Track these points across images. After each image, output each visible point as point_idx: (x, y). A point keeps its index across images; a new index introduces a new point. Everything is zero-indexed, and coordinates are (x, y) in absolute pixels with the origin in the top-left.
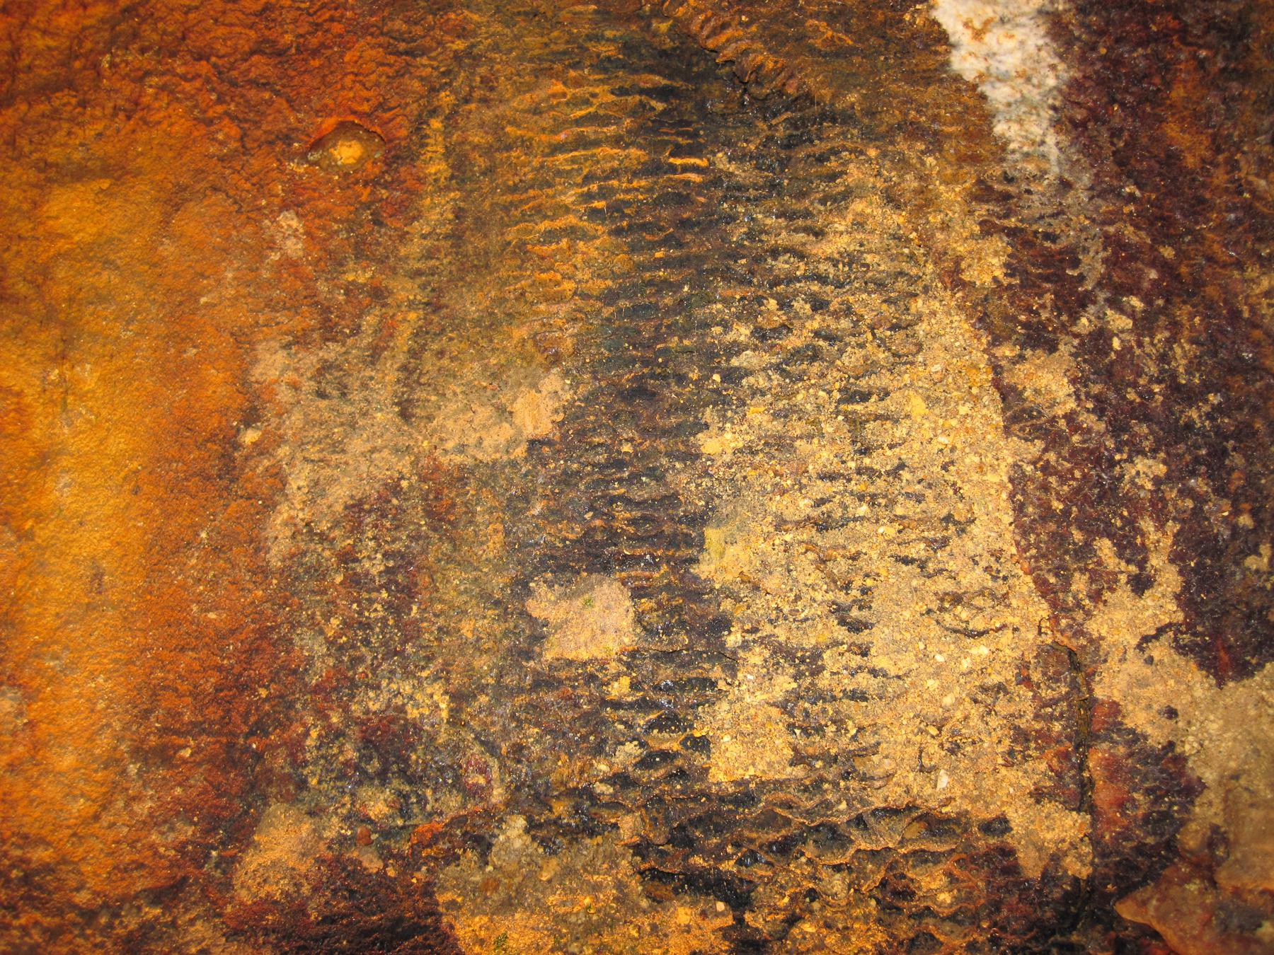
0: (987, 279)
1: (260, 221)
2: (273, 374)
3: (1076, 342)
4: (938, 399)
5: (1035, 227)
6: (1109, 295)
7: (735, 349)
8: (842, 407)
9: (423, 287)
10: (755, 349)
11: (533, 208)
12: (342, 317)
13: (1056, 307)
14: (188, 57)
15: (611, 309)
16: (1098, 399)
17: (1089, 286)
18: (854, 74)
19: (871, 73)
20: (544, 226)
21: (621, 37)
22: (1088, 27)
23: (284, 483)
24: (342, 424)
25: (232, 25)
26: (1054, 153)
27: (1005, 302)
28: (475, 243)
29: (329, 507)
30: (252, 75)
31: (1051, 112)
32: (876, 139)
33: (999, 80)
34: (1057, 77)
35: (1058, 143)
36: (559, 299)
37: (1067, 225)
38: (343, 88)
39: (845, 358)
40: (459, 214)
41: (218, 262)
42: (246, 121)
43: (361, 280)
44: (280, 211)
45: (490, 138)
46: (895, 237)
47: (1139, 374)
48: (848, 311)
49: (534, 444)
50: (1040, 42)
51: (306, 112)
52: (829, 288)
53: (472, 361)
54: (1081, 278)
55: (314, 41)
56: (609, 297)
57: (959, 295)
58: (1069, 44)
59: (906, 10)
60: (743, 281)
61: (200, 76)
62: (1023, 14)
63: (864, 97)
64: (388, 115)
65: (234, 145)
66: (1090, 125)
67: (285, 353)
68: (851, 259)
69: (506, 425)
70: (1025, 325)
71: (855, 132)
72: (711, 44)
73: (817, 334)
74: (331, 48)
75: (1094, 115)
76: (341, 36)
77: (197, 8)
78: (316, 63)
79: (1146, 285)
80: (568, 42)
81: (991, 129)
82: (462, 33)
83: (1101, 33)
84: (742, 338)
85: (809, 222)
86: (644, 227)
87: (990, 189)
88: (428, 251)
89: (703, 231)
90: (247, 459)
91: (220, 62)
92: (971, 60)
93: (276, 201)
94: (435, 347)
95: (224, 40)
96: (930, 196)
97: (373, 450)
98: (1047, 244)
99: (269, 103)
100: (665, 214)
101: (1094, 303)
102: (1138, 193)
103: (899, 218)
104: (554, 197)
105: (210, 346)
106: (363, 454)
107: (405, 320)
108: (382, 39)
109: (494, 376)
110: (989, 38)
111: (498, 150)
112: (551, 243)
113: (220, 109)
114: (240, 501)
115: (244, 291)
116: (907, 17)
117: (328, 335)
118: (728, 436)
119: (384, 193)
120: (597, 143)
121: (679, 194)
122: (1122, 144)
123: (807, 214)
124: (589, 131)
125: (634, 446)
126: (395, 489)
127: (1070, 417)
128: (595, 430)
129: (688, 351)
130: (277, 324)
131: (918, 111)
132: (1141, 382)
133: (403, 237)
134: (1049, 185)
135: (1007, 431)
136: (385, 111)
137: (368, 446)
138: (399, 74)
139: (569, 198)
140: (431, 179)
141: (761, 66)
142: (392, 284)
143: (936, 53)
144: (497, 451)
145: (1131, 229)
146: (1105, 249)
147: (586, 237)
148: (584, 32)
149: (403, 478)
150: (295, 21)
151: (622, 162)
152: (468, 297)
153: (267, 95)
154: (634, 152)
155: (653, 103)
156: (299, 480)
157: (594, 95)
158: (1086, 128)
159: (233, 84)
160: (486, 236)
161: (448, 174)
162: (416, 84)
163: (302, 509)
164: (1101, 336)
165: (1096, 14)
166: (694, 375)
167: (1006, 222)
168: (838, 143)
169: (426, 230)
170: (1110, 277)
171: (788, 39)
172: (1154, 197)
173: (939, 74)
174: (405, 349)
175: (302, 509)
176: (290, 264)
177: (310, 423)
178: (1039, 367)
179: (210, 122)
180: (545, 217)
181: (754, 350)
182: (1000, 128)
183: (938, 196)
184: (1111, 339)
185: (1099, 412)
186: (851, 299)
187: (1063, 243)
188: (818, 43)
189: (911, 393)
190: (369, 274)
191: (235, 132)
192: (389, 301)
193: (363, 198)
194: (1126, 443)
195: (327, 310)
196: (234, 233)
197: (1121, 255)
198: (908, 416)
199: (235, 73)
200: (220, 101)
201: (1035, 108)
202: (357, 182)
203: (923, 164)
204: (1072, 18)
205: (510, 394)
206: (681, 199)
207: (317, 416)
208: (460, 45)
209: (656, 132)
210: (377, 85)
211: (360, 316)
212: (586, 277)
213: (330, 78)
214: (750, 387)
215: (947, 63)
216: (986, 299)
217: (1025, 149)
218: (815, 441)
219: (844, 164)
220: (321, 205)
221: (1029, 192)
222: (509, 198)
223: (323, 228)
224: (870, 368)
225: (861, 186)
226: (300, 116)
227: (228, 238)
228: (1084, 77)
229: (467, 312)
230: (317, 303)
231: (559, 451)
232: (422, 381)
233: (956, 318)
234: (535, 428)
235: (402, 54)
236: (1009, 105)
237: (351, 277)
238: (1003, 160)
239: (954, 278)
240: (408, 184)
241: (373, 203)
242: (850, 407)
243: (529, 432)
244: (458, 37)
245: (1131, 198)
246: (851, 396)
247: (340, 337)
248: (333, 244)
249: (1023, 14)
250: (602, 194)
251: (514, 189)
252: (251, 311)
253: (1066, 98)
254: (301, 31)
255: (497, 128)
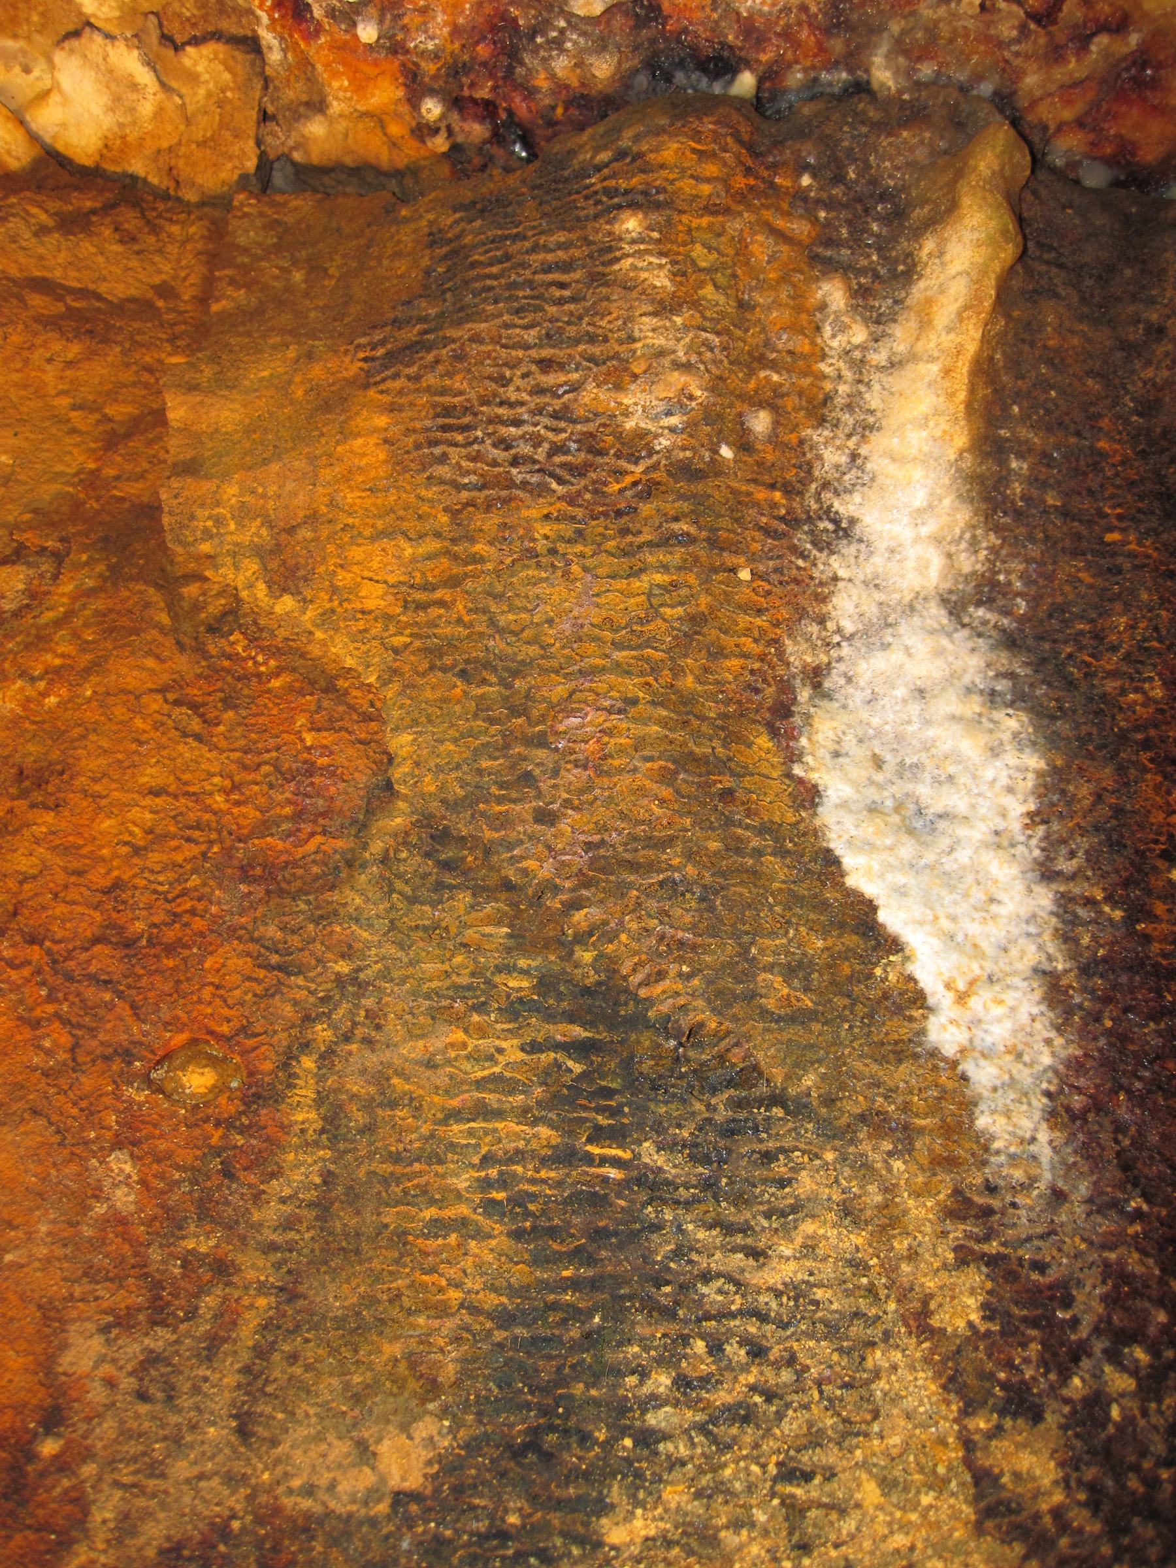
0: (961, 1324)
1: (87, 1160)
2: (86, 1365)
3: (1067, 1409)
4: (895, 1483)
5: (1020, 1252)
6: (1107, 1344)
7: (654, 1401)
8: (779, 1488)
9: (278, 1266)
10: (676, 1405)
11: (418, 1186)
12: (176, 1296)
13: (1043, 1362)
14: (18, 938)
15: (505, 1334)
16: (1093, 1488)
17: (1084, 1332)
18: (812, 1046)
19: (834, 1044)
20: (430, 1213)
21: (537, 968)
22: (1093, 991)
23: (86, 1512)
24: (165, 1439)
25: (74, 903)
26: (1045, 1153)
27: (982, 1355)
28: (344, 1219)
29: (140, 1549)
30: (92, 969)
31: (1045, 1100)
32: (834, 1137)
33: (984, 1055)
34: (1053, 1054)
35: (1051, 1142)
36: (442, 1311)
37: (1060, 1250)
38: (200, 1001)
39: (785, 1425)
40: (328, 1178)
41: (31, 1210)
42: (80, 1026)
43: (203, 1249)
44: (112, 1150)
45: (372, 1090)
46: (851, 1263)
47: (1144, 1453)
48: (792, 1360)
49: (400, 1498)
50: (1035, 1010)
51: (154, 1024)
52: (769, 1328)
53: (331, 1374)
54: (1075, 1322)
55: (170, 935)
56: (505, 1319)
57: (926, 1345)
58: (1069, 1012)
59: (876, 964)
60: (669, 1314)
61: (29, 963)
62: (1015, 973)
63: (824, 1077)
64: (251, 1042)
65: (62, 1056)
66: (1091, 1117)
67: (103, 1339)
68: (797, 1292)
69: (366, 1470)
70: (1005, 1386)
71: (810, 1126)
72: (643, 993)
73: (753, 1388)
74: (188, 947)
75: (1097, 1105)
76: (202, 934)
77: (34, 877)
78: (171, 963)
79: (1152, 1331)
80: (473, 975)
81: (972, 1121)
82: (347, 954)
83: (1107, 1000)
84: (662, 1389)
85: (749, 1241)
86: (552, 1232)
87: (968, 1202)
88: (287, 1220)
89: (620, 1247)
90: (42, 1474)
91: (55, 948)
92: (952, 1029)
93: (108, 1135)
94: (286, 1348)
95: (63, 921)
96: (896, 1212)
97: (201, 1477)
98: (1035, 1276)
99: (110, 1007)
100: (577, 1220)
101: (1090, 1355)
102: (1145, 1207)
103: (858, 1239)
104: (443, 1176)
105: (12, 1319)
106: (188, 1481)
107: (252, 1306)
108: (251, 947)
109: (357, 1399)
110: (975, 1002)
111: (380, 1105)
112: (436, 1236)
113: (50, 1008)
114: (28, 1533)
115: (60, 1252)
116: (878, 972)
117: (157, 1317)
118: (638, 1523)
119: (240, 1140)
120: (499, 1114)
121: (595, 1194)
122: (1127, 1142)
123: (746, 1229)
124: (492, 1099)
125: (522, 1516)
126: (222, 1531)
127: (1057, 1513)
128: (475, 1487)
129: (597, 1403)
130: (97, 1299)
131: (886, 1097)
132: (1147, 1465)
133: (258, 1197)
134: (1040, 1196)
135: (979, 1529)
136: (248, 1036)
137: (196, 1470)
138: (268, 995)
139: (462, 1182)
140: (297, 1128)
141: (701, 1025)
142: (240, 1258)
143: (911, 1019)
144: (354, 1501)
145: (1136, 1256)
146: (1104, 1282)
147: (480, 1235)
148: (493, 963)
149: (234, 1517)
150: (149, 907)
151: (528, 1142)
152: (332, 1287)
153: (107, 997)
154: (544, 1131)
155: (570, 1064)
156: (105, 1512)
157: (500, 1051)
158: (1086, 1121)
159: (69, 977)
160: (358, 1213)
161: (319, 1125)
162: (288, 1010)
163: (105, 1551)
164: (1097, 1401)
165: (1102, 976)
166: (601, 1435)
167: (985, 1248)
168: (788, 1142)
169: (287, 1192)
170: (1109, 1321)
171: (736, 997)
172: (1164, 1212)
173: (908, 1049)
174: (250, 1343)
175: (105, 1551)
176: (120, 1221)
177: (126, 1434)
178: (1020, 1446)
179: (36, 1024)
180: (432, 1202)
181: (675, 1406)
182: (983, 1121)
183: (905, 1212)
184: (1109, 1405)
185: (1094, 1505)
186: (795, 1345)
187: (1053, 1274)
188: (770, 1004)
189: (864, 1476)
190: (212, 1243)
191: (65, 1040)
192: (235, 1279)
193: (214, 1141)
194: (1127, 1549)
195: (158, 1285)
196: (53, 1172)
197: (1122, 1288)
198: (858, 1506)
199: (71, 964)
200: (50, 999)
201: (1026, 1094)
202: (206, 1120)
203: (889, 1169)
204: (1070, 979)
205: (375, 1429)
206: (597, 1201)
207: (135, 1425)
208: (343, 967)
209: (571, 1102)
210: (242, 1003)
211: (197, 1296)
212: (477, 1287)
213: (184, 986)
214: (669, 1456)
215: (923, 1032)
216: (958, 1351)
217: (1012, 1149)
218: (744, 1532)
219: (796, 1169)
220: (162, 1146)
221: (1014, 1205)
222: (388, 1168)
223: (161, 1176)
224: (814, 1439)
225: (813, 1198)
226: (146, 1027)
227: (45, 1178)
228: (1086, 1055)
229: (329, 1308)
230: (146, 1275)
231: (430, 1509)
232: (269, 1389)
233: (921, 1375)
234: (403, 1479)
235: (273, 968)
236: (995, 1089)
237: (190, 1244)
238: (985, 1163)
239: (920, 1321)
240: (269, 1131)
241: (225, 1149)
242: (789, 1489)
243: (395, 1481)
244: (343, 956)
245: (1138, 1215)
246: (790, 1473)
247: (171, 1320)
248: (173, 1198)
249: (1015, 973)
250: (503, 1182)
251: (396, 1158)
252: (65, 1279)
253: (1063, 1080)
254: (156, 919)
255: (381, 1079)
